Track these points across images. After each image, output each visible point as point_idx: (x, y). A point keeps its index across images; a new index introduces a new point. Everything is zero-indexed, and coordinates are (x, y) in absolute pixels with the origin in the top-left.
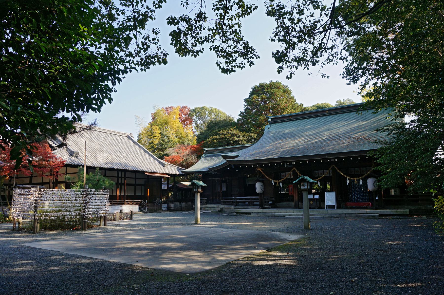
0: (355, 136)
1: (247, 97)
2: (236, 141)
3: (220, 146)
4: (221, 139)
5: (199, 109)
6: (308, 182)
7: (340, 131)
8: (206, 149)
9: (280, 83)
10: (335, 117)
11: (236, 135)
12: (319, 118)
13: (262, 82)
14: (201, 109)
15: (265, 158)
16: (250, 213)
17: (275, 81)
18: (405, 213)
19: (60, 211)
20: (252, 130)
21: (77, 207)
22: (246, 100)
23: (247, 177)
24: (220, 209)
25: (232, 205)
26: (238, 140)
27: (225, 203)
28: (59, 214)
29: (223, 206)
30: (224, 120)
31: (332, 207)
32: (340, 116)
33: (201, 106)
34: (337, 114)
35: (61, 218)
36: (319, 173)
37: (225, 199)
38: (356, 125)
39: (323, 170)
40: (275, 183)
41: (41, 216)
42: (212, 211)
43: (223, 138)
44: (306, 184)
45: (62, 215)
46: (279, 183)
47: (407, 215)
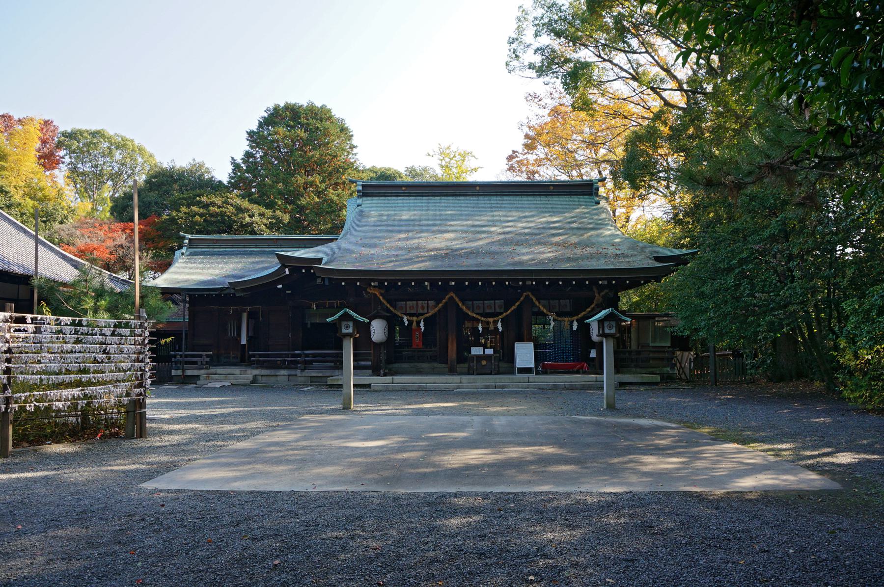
0: (556, 239)
1: (254, 127)
2: (248, 225)
3: (209, 233)
4: (211, 215)
5: (86, 134)
6: (356, 322)
7: (519, 227)
8: (189, 236)
9: (329, 111)
10: (495, 200)
11: (248, 210)
12: (462, 198)
13: (292, 100)
14: (94, 134)
15: (406, 268)
16: (369, 386)
17: (318, 104)
18: (654, 381)
19: (78, 384)
20: (276, 203)
21: (125, 371)
22: (251, 134)
23: (310, 307)
24: (251, 377)
25: (279, 368)
26: (252, 223)
27: (261, 365)
28: (76, 392)
29: (257, 372)
30: (191, 172)
31: (527, 371)
32: (503, 200)
33: (93, 128)
34: (496, 195)
35: (82, 403)
36: (420, 306)
37: (261, 356)
38: (543, 220)
39: (559, 299)
40: (410, 322)
41: (25, 402)
42: (234, 382)
43: (217, 214)
44: (351, 325)
45: (85, 396)
46: (418, 323)
47: (657, 384)
